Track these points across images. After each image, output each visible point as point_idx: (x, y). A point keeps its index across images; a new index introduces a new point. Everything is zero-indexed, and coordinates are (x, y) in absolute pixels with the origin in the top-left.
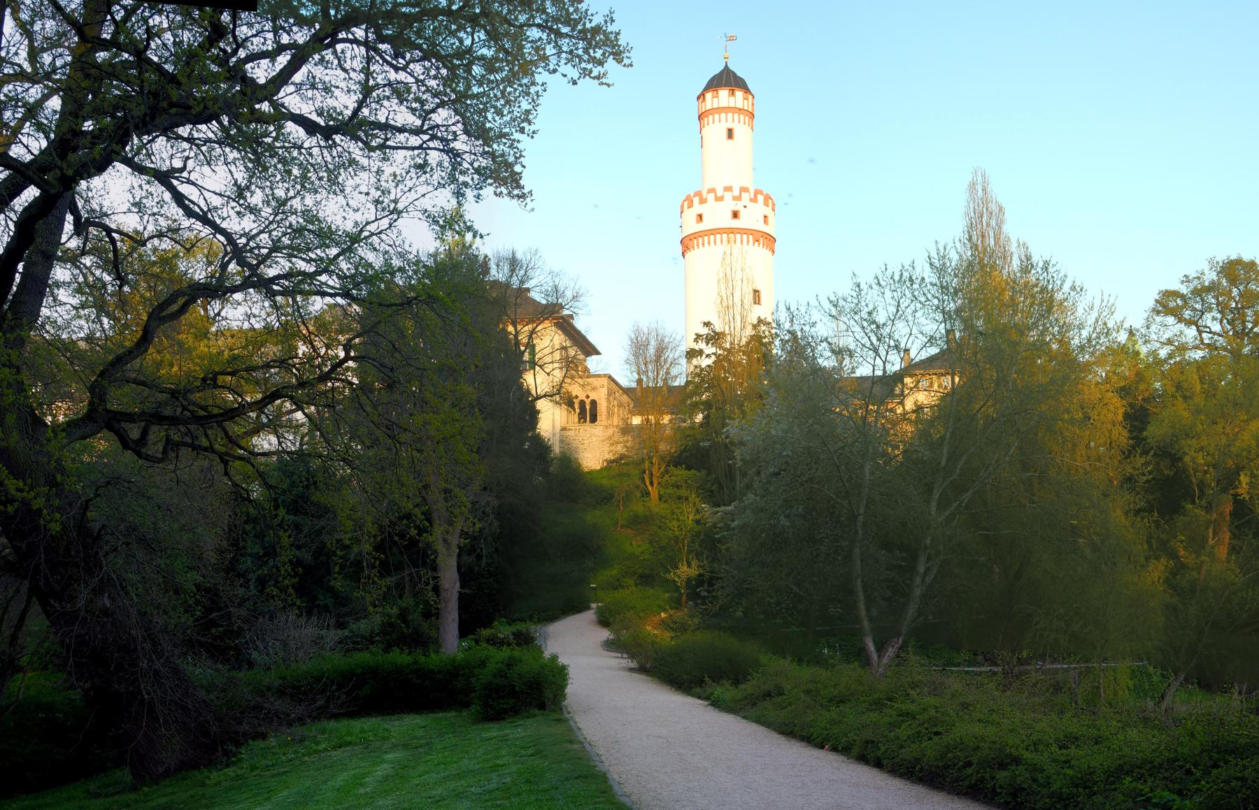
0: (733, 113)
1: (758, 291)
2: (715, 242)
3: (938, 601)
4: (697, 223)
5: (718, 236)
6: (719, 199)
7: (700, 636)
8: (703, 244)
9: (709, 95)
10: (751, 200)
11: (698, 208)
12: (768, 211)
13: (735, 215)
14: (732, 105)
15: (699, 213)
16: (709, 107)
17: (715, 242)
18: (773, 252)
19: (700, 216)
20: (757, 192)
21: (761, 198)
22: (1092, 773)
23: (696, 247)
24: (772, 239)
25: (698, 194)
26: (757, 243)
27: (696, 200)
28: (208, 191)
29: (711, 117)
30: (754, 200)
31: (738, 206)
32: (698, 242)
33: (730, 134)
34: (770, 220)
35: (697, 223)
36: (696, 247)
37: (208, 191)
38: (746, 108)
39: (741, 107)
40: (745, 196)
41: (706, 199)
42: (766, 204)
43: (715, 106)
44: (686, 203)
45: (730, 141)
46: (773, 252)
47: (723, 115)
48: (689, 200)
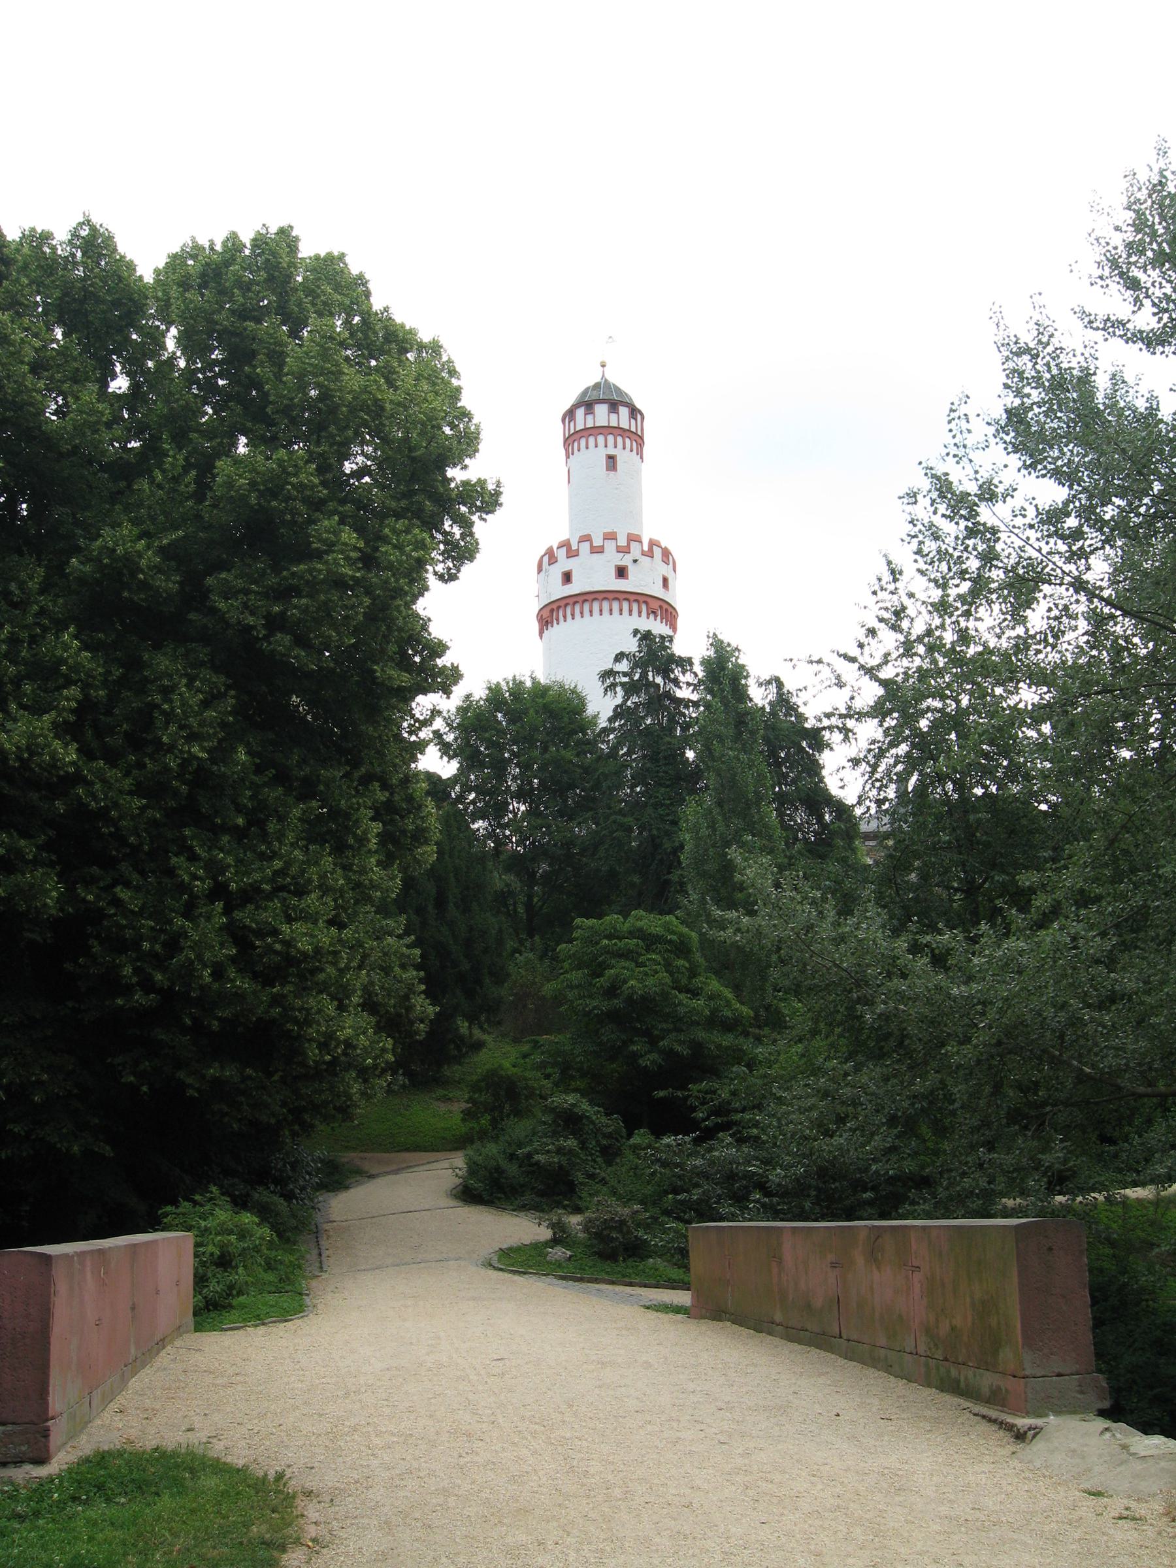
6: (597, 550)
9: (580, 412)
13: (621, 572)
14: (614, 424)
21: (657, 552)
30: (650, 554)
31: (626, 561)
33: (611, 459)
44: (546, 559)
45: (612, 473)
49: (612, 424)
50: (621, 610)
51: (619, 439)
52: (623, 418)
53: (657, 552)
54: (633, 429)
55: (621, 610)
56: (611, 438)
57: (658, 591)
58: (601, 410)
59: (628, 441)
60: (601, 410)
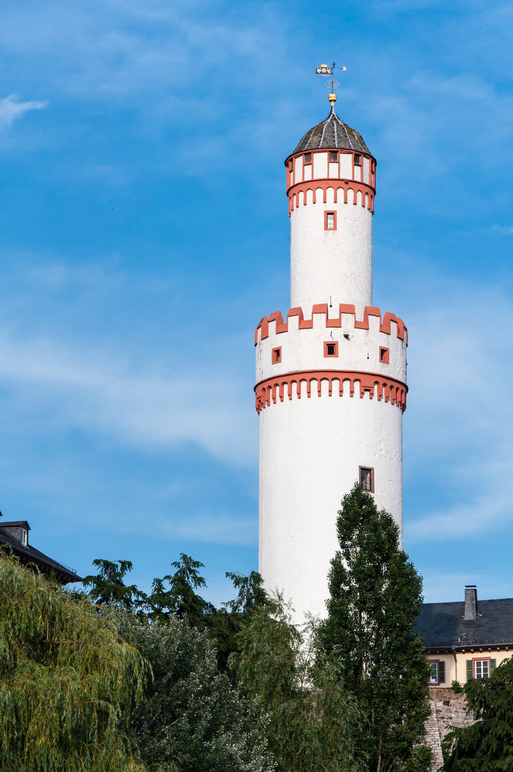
2: (299, 394)
3: (40, 607)
4: (273, 363)
8: (281, 397)
10: (357, 325)
14: (334, 175)
15: (276, 346)
16: (299, 180)
17: (299, 394)
18: (403, 407)
19: (277, 352)
21: (394, 326)
23: (278, 399)
24: (401, 388)
26: (367, 394)
28: (456, 669)
29: (301, 195)
30: (363, 325)
32: (282, 391)
35: (273, 363)
36: (278, 399)
37: (456, 669)
38: (358, 178)
39: (336, 177)
40: (348, 321)
41: (311, 322)
42: (385, 330)
43: (308, 178)
46: (403, 407)
47: (319, 192)
50: (352, 392)
51: (350, 193)
53: (394, 326)
54: (367, 182)
55: (352, 392)
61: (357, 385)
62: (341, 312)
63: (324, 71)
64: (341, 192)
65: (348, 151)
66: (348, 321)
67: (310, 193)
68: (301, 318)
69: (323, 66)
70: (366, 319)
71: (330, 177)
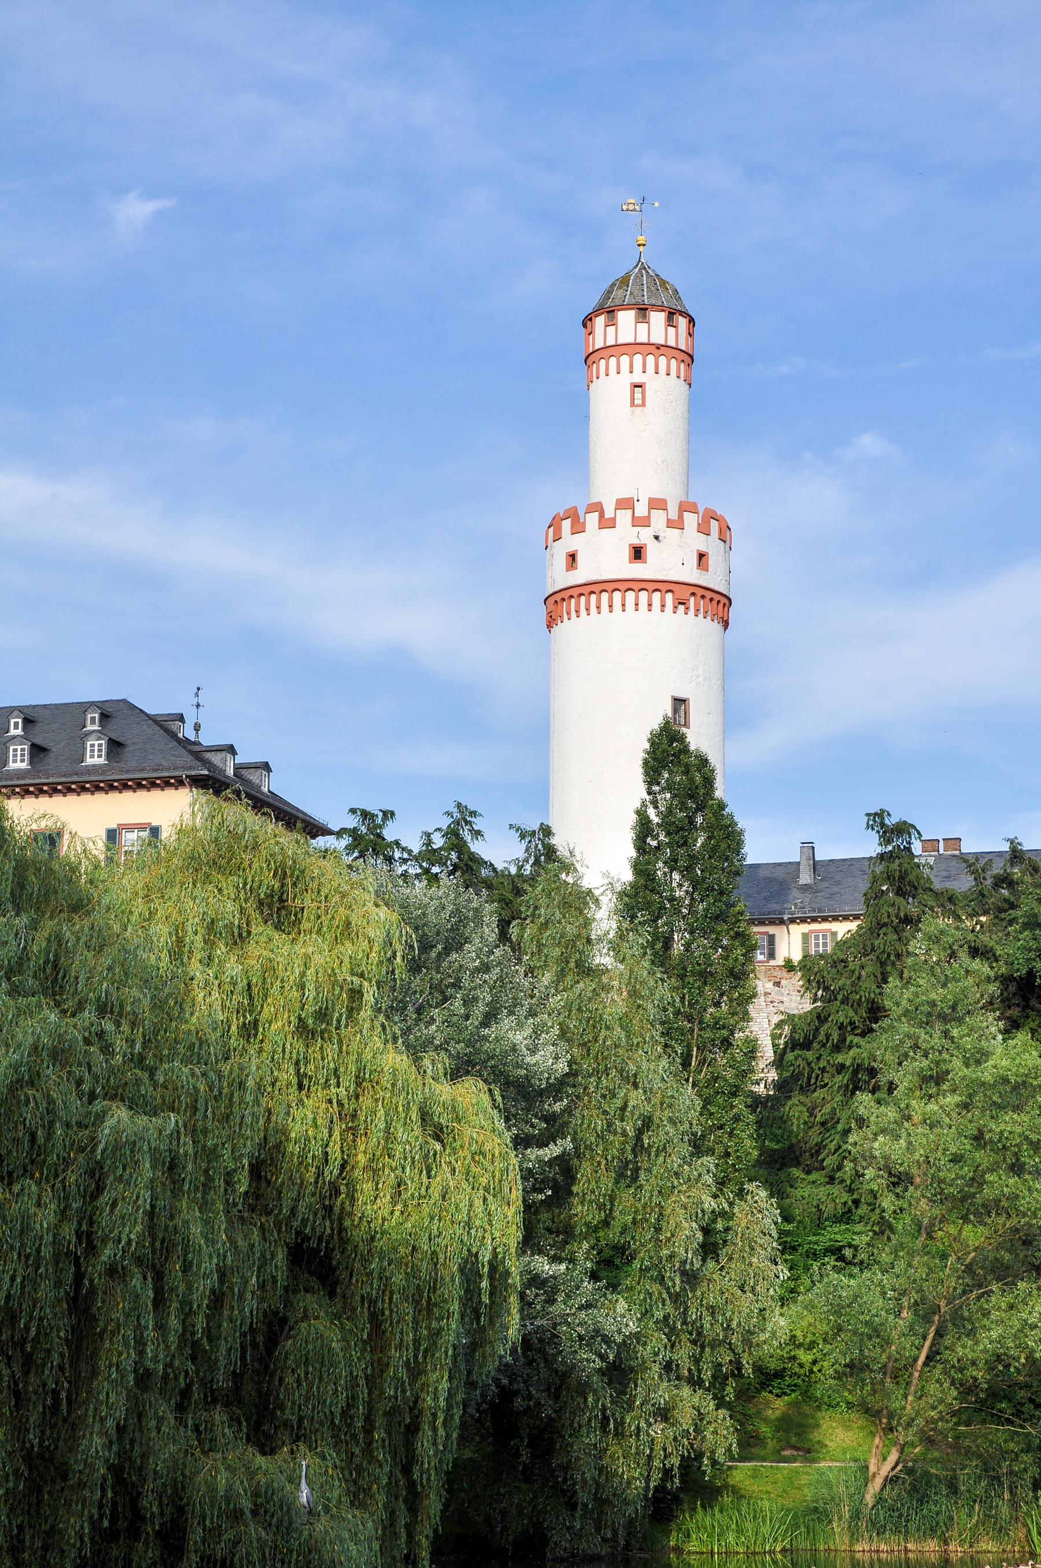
0: (631, 357)
1: (684, 701)
2: (598, 608)
5: (643, 596)
6: (607, 523)
7: (513, 1333)
9: (600, 321)
10: (670, 524)
11: (570, 542)
12: (711, 544)
13: (638, 553)
14: (642, 338)
15: (571, 549)
16: (599, 344)
17: (598, 608)
18: (726, 624)
19: (572, 557)
20: (686, 507)
21: (714, 525)
22: (94, 1255)
23: (573, 614)
24: (724, 600)
25: (573, 514)
26: (681, 608)
27: (566, 525)
30: (677, 524)
31: (644, 537)
32: (578, 604)
34: (712, 561)
36: (573, 614)
38: (672, 342)
39: (646, 341)
40: (658, 519)
41: (614, 519)
43: (610, 341)
44: (566, 525)
46: (726, 624)
48: (555, 523)
49: (669, 344)
50: (663, 606)
51: (663, 360)
52: (677, 336)
53: (714, 525)
56: (663, 360)
57: (690, 574)
58: (626, 318)
59: (673, 362)
60: (626, 318)
61: (669, 597)
62: (650, 508)
63: (631, 207)
64: (650, 359)
65: (660, 308)
66: (658, 519)
67: (613, 361)
68: (602, 515)
69: (630, 201)
70: (681, 517)
71: (638, 341)
